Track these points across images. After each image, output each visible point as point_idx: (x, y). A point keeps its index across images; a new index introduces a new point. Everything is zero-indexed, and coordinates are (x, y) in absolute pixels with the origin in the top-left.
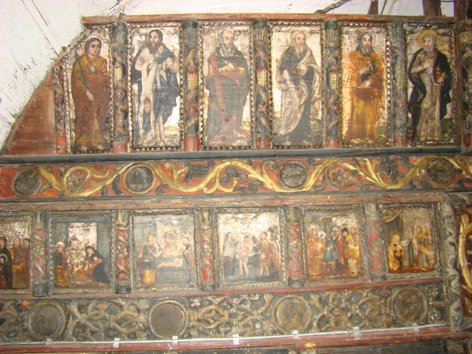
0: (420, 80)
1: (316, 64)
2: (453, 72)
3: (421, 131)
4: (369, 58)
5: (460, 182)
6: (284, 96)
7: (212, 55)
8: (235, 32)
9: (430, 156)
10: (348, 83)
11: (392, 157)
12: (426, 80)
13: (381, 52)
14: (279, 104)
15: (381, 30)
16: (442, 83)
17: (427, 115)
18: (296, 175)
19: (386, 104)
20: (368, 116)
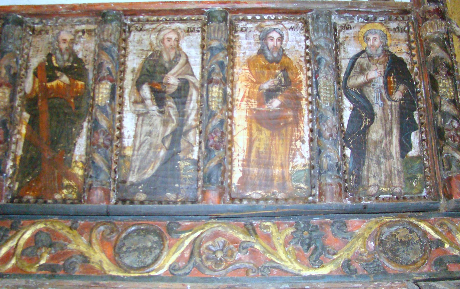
0: (363, 96)
1: (193, 75)
2: (417, 83)
3: (368, 178)
4: (278, 66)
5: (440, 262)
6: (140, 122)
7: (41, 65)
8: (77, 32)
9: (386, 219)
10: (244, 103)
11: (316, 220)
12: (374, 96)
13: (297, 56)
14: (132, 134)
15: (297, 25)
16: (400, 100)
17: (378, 152)
18: (145, 248)
19: (306, 135)
20: (277, 154)
